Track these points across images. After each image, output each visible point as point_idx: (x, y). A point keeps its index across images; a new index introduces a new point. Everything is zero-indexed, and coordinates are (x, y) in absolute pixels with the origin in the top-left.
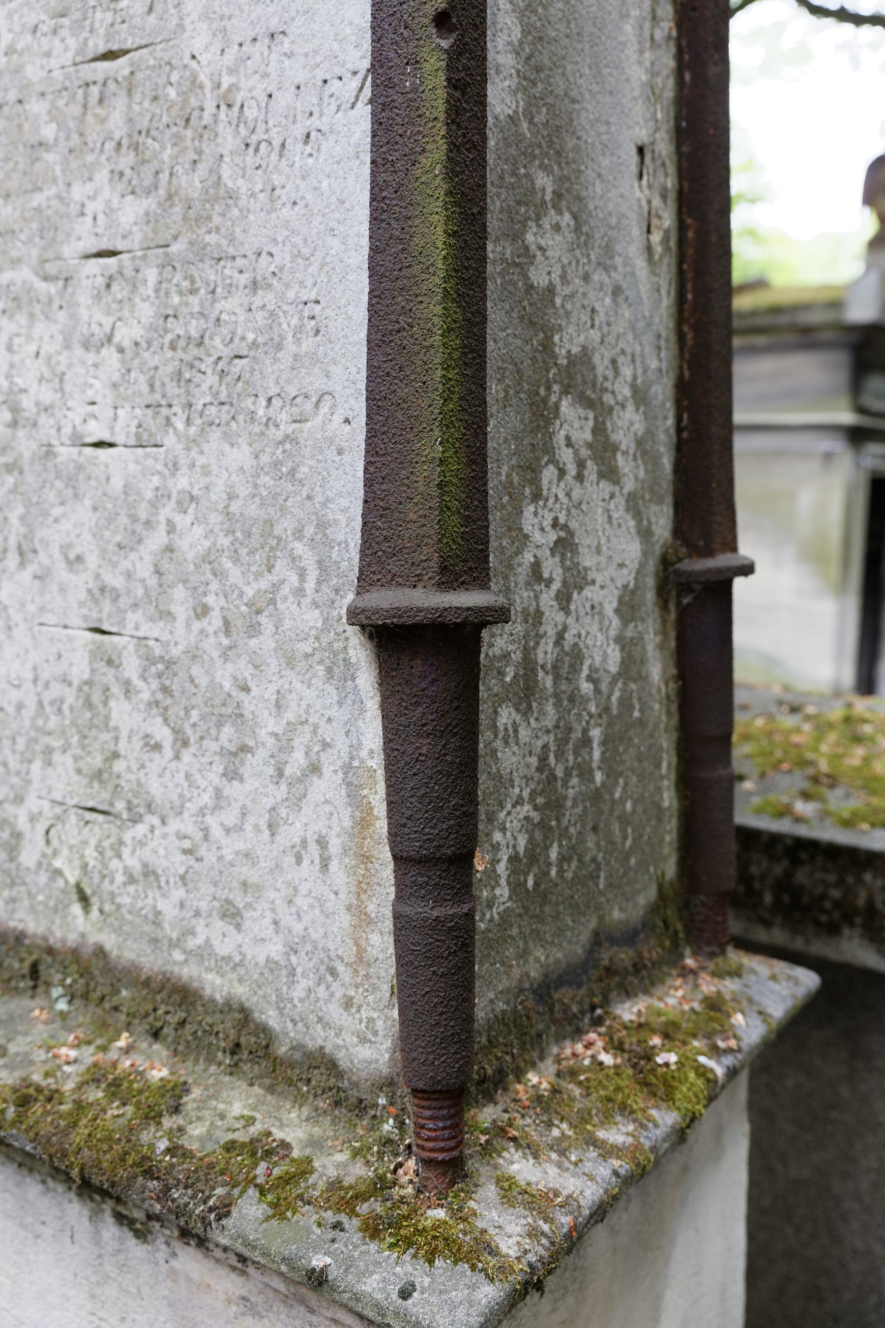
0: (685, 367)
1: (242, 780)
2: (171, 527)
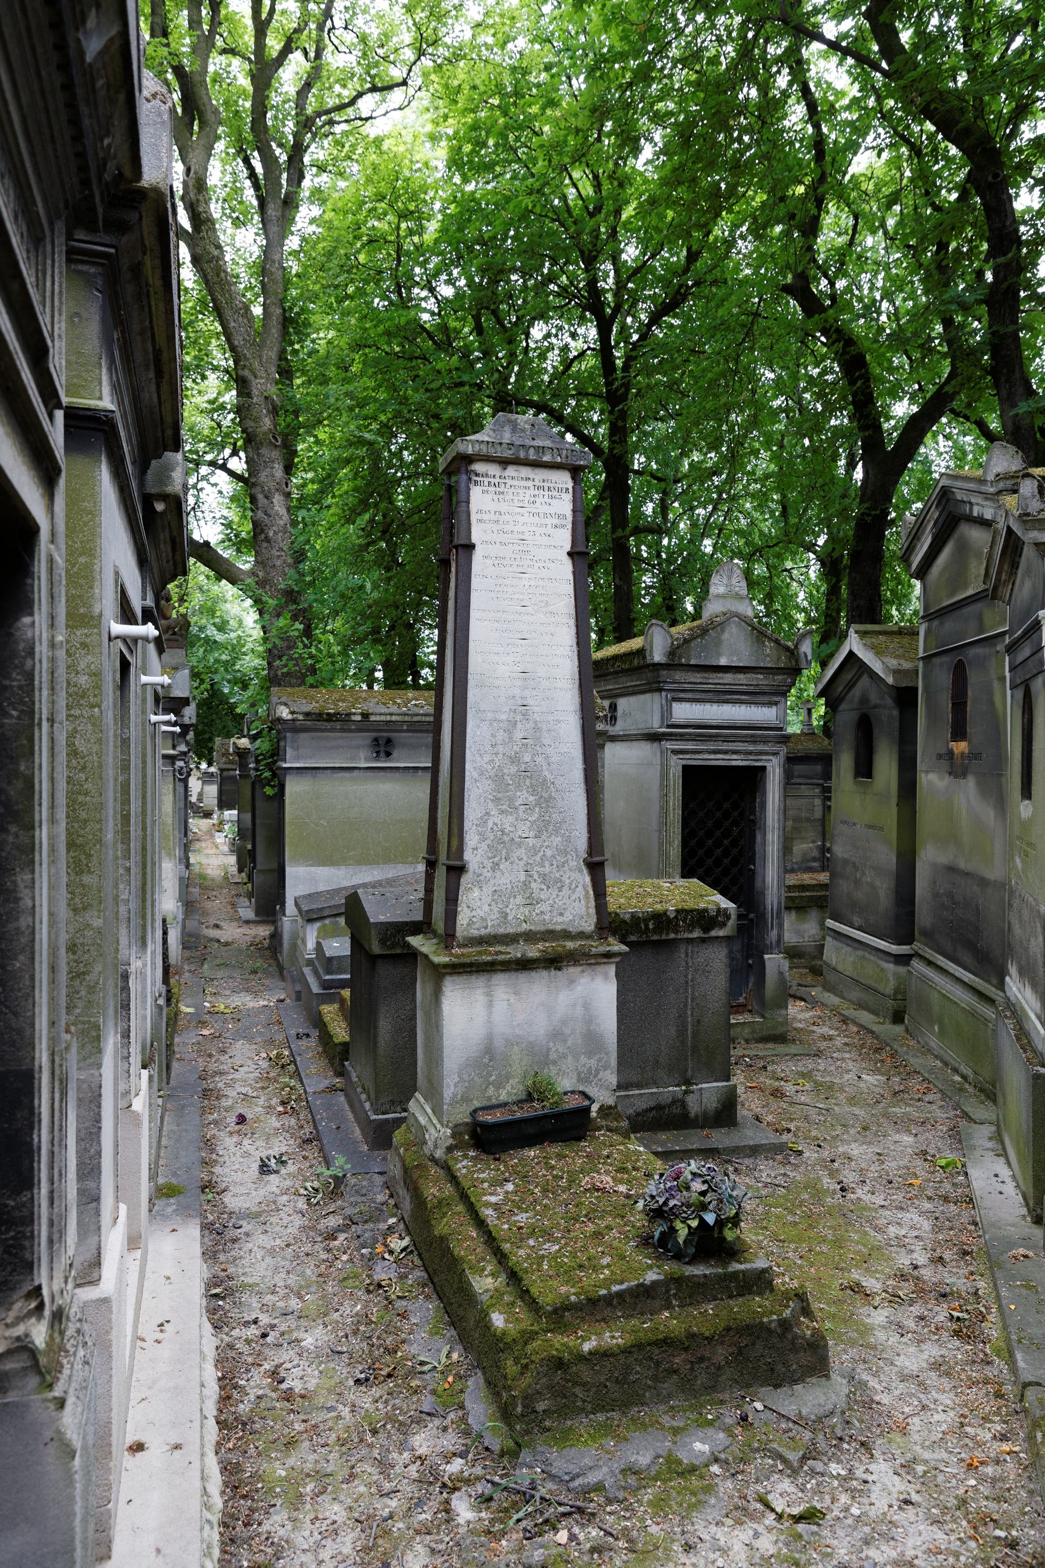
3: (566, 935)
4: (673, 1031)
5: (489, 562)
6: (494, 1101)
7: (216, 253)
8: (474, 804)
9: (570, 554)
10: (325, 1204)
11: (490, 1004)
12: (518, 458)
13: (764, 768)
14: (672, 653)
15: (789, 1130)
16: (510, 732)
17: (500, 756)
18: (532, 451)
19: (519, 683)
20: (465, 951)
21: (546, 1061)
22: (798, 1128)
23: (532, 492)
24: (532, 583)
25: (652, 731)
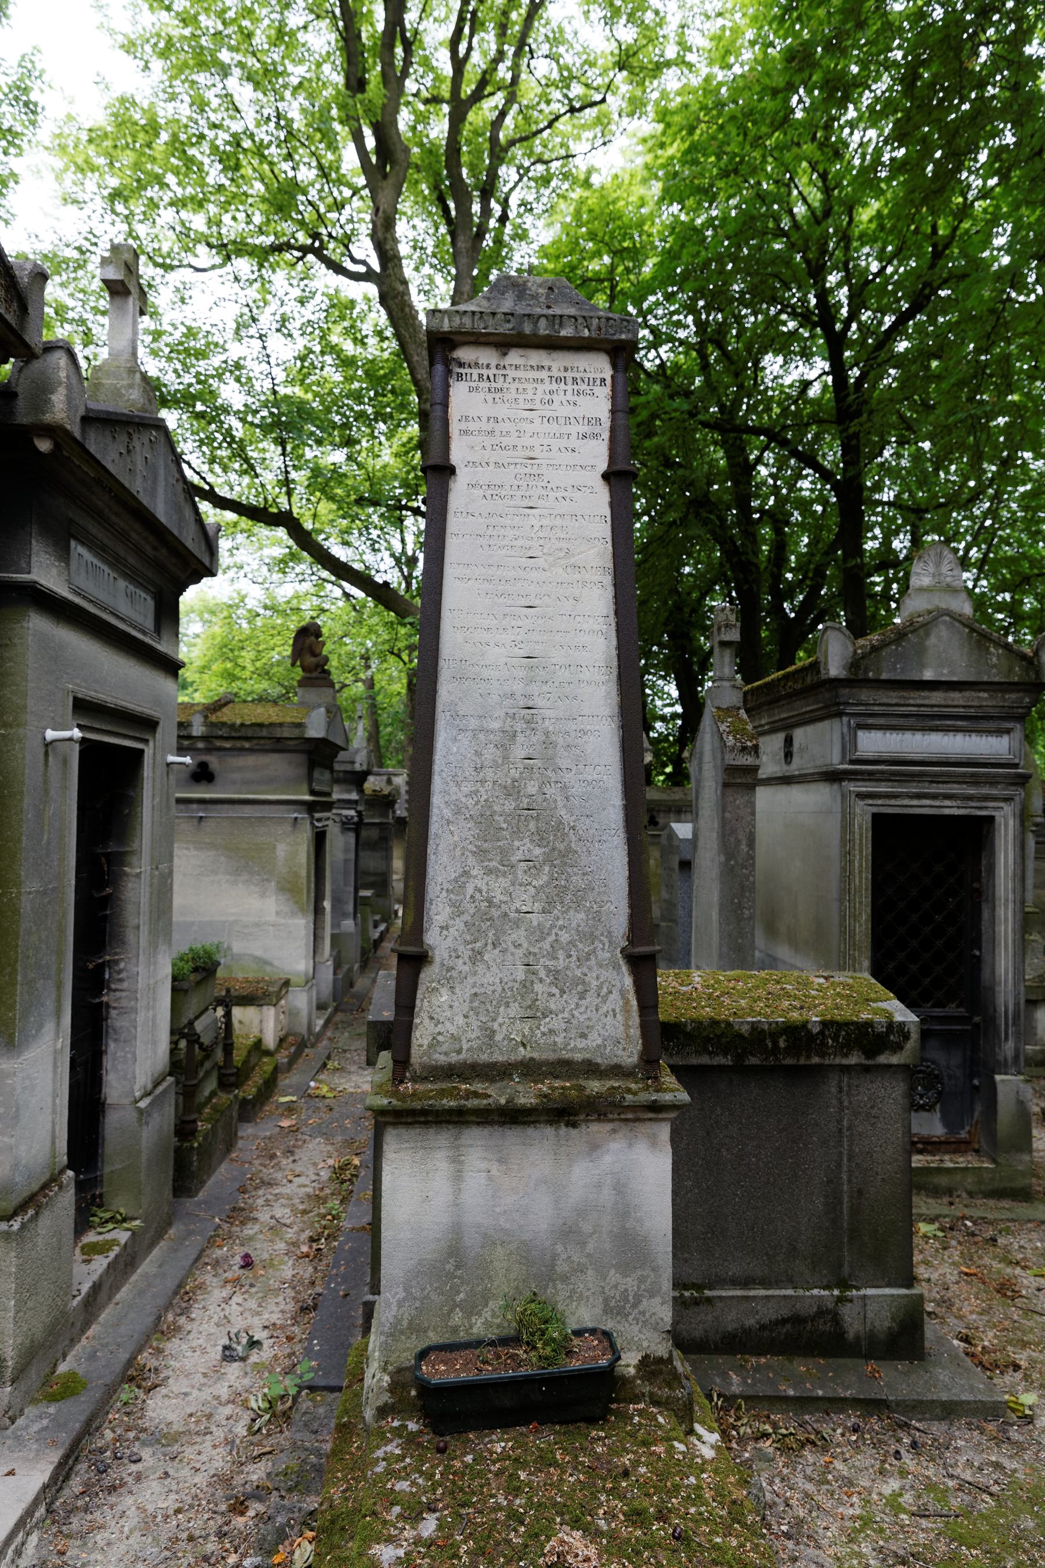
0: (1031, 841)
1: (242, 1267)
2: (557, 935)
3: (591, 1069)
4: (819, 1202)
5: (478, 492)
6: (462, 1336)
7: (401, 288)
8: (445, 859)
9: (606, 476)
10: (269, 1435)
11: (458, 1177)
12: (520, 334)
13: (992, 819)
14: (855, 664)
15: (1017, 1367)
16: (504, 748)
17: (489, 785)
18: (543, 323)
19: (521, 673)
20: (421, 1087)
21: (550, 1275)
22: (1032, 1361)
23: (547, 386)
24: (545, 522)
25: (831, 768)
